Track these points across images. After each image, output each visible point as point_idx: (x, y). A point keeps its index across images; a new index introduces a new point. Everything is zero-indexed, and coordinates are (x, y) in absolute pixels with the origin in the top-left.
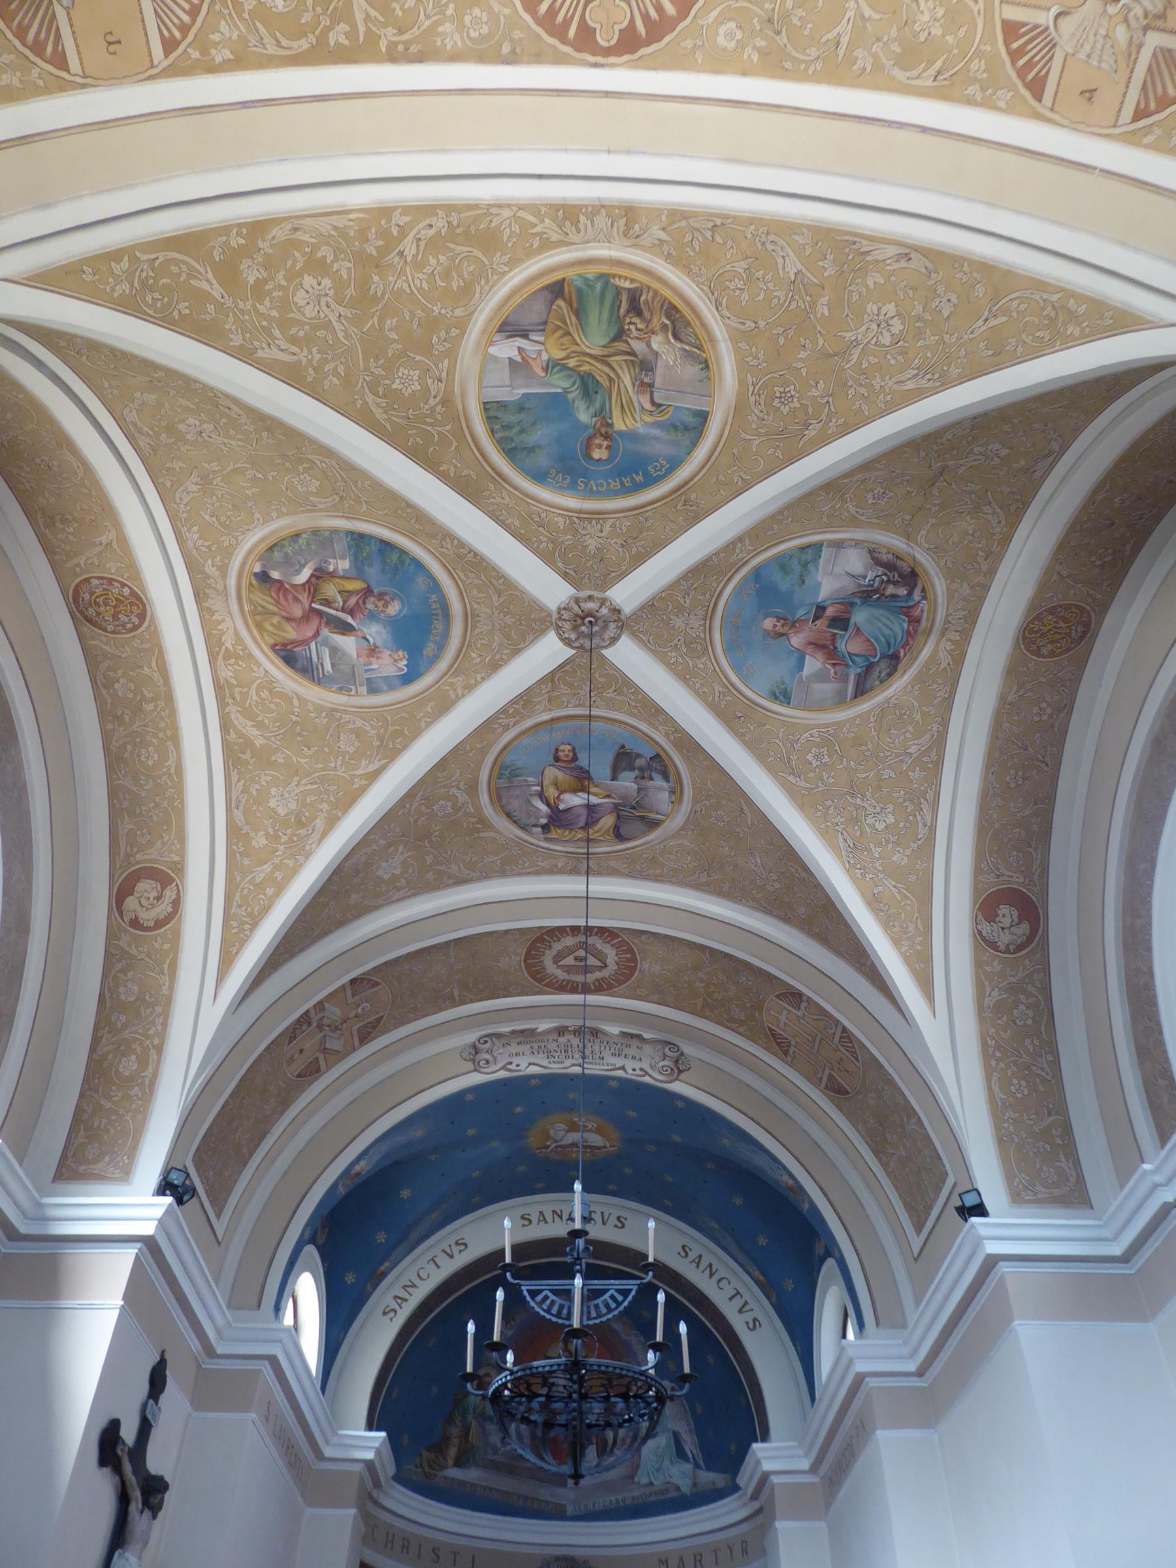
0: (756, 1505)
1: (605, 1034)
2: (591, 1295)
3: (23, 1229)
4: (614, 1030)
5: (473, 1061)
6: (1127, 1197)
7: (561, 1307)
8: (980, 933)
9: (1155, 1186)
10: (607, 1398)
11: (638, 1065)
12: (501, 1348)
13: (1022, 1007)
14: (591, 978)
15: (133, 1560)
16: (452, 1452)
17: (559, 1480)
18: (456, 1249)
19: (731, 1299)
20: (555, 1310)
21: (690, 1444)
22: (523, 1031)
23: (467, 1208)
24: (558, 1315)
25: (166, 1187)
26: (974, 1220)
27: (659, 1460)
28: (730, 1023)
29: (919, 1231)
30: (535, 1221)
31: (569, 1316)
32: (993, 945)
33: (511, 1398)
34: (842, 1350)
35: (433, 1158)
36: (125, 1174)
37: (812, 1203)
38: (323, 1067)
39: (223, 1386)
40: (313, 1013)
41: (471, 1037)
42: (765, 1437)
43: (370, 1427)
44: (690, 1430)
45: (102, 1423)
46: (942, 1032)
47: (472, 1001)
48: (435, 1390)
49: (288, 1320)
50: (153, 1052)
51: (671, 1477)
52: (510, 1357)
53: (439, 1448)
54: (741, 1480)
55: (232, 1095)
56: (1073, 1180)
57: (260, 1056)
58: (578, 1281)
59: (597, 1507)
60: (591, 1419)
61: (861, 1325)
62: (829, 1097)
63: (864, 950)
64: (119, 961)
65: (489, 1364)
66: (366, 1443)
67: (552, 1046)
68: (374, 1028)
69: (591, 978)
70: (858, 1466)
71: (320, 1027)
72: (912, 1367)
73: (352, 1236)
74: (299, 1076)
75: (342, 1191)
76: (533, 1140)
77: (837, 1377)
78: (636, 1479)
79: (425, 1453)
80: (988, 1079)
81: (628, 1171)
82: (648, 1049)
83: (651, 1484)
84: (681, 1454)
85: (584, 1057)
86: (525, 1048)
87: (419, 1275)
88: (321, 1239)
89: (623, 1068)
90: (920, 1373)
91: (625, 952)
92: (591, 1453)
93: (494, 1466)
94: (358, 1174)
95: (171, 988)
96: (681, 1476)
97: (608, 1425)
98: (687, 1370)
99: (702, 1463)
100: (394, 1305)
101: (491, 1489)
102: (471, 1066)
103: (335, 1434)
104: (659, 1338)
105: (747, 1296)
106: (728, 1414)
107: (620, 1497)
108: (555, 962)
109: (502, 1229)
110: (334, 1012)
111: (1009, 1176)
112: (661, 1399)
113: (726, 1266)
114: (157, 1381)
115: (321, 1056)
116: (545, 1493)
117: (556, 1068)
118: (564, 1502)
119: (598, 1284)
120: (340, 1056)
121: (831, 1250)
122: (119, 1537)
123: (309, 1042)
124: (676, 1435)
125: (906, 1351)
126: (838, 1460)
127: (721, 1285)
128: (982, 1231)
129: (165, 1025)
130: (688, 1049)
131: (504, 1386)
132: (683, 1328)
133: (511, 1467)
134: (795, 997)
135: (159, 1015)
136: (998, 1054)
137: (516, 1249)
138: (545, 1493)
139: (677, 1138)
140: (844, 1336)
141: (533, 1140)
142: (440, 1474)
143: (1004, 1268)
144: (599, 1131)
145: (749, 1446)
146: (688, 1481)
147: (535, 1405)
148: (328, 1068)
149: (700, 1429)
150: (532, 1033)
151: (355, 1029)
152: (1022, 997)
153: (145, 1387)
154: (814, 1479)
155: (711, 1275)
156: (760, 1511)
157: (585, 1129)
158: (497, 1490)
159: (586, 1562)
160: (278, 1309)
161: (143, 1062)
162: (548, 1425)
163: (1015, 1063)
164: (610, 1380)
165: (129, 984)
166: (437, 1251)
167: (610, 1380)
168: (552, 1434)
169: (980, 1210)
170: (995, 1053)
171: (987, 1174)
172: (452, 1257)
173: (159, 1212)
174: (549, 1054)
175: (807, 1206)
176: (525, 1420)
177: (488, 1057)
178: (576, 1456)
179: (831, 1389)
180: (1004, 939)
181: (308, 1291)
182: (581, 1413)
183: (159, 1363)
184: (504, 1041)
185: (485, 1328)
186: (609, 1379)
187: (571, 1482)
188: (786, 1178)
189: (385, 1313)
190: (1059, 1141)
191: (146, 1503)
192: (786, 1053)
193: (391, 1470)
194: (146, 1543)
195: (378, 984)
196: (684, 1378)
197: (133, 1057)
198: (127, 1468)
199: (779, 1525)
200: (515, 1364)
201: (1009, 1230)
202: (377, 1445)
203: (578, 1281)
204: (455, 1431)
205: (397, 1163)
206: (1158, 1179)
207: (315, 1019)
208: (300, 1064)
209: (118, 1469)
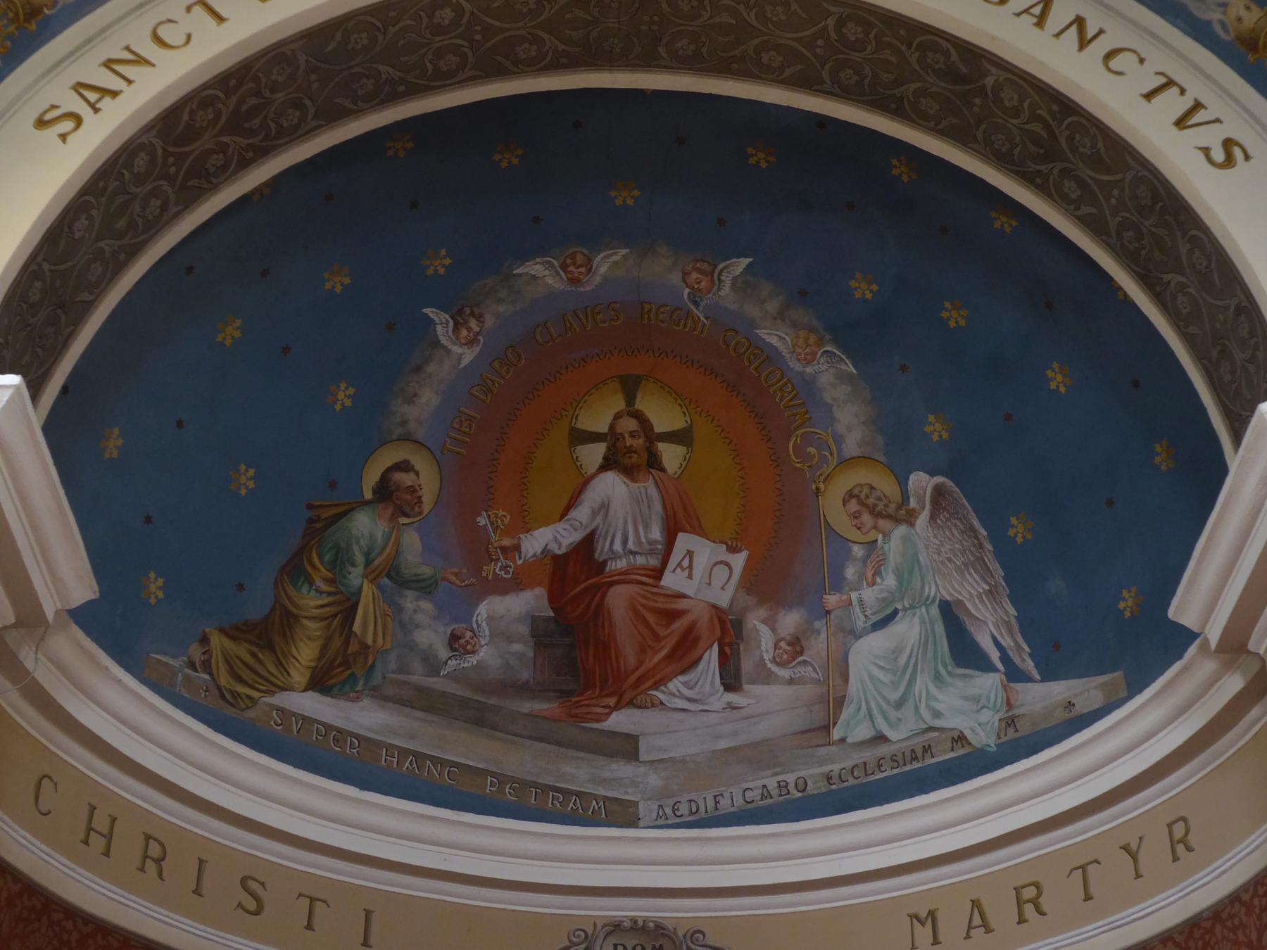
16: (305, 653)
19: (1149, 96)
21: (992, 625)
48: (246, 479)
51: (937, 714)
53: (268, 633)
54: (1185, 608)
59: (725, 803)
65: (407, 438)
78: (836, 734)
83: (881, 739)
84: (965, 652)
93: (428, 702)
99: (1029, 665)
105: (1197, 89)
107: (791, 778)
124: (951, 614)
127: (1115, 64)
146: (991, 718)
149: (1022, 585)
158: (436, 761)
159: (696, 934)
189: (41, 123)
204: (310, 601)
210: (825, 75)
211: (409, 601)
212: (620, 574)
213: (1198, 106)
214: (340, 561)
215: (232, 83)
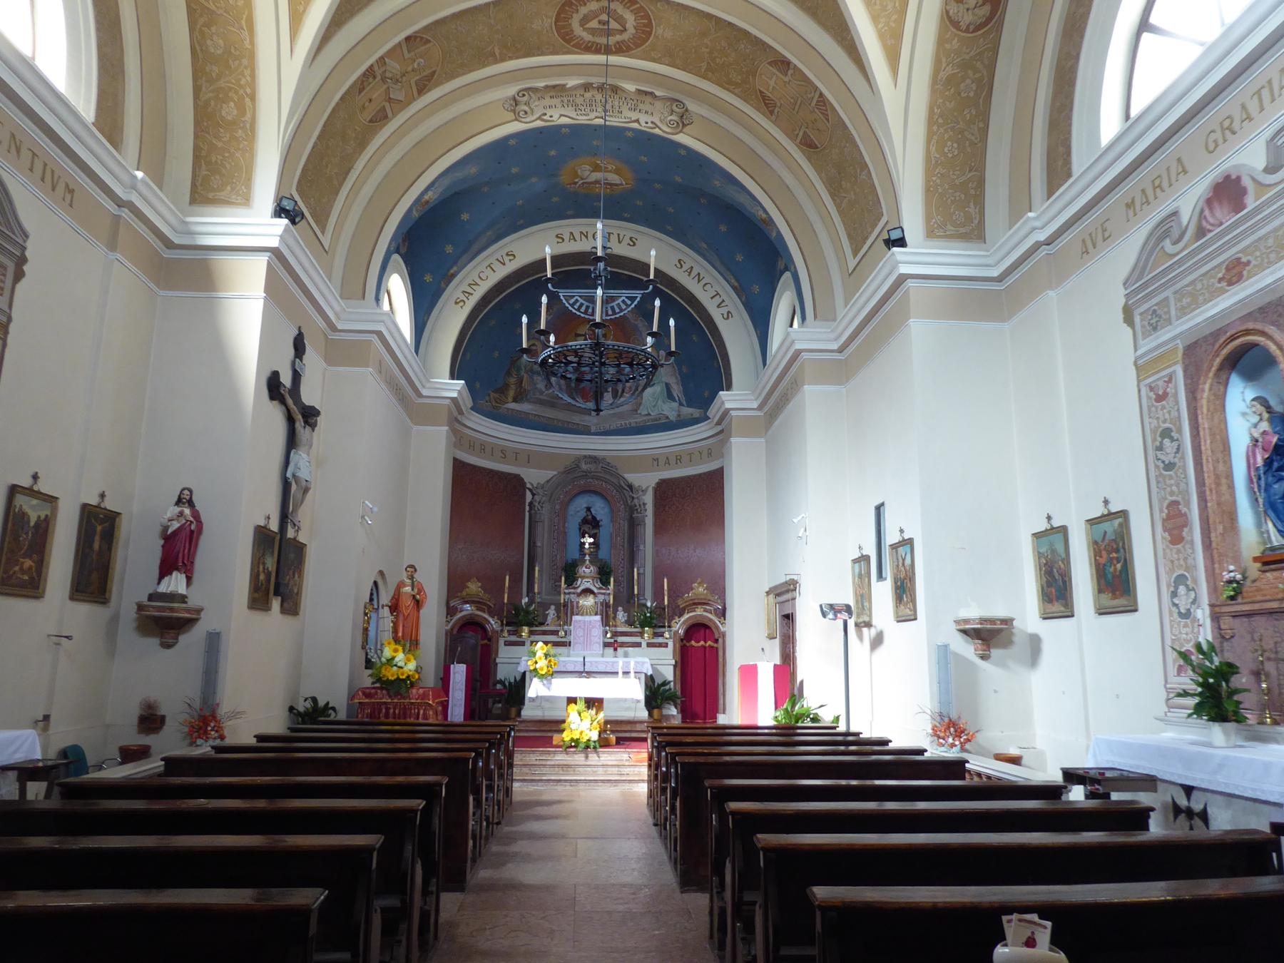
0: (719, 428)
1: (623, 90)
2: (606, 301)
3: (177, 241)
4: (631, 87)
5: (514, 111)
6: (1016, 232)
7: (588, 307)
8: (947, 12)
9: (1035, 229)
10: (618, 365)
11: (649, 119)
12: (545, 333)
13: (968, 81)
14: (612, 40)
15: (304, 455)
16: (511, 393)
17: (586, 412)
18: (507, 259)
20: (583, 309)
21: (677, 391)
22: (554, 87)
23: (515, 228)
24: (586, 313)
25: (280, 211)
26: (895, 249)
27: (654, 400)
28: (727, 84)
29: (855, 255)
30: (567, 239)
31: (593, 314)
32: (956, 24)
33: (554, 364)
34: (788, 334)
35: (486, 189)
36: (245, 200)
37: (779, 233)
38: (390, 115)
39: (346, 351)
40: (376, 68)
41: (511, 90)
42: (729, 387)
43: (452, 377)
45: (267, 374)
46: (899, 103)
47: (511, 58)
48: (496, 354)
49: (386, 307)
50: (247, 100)
52: (552, 338)
53: (503, 390)
55: (319, 138)
56: (976, 222)
57: (337, 104)
58: (599, 292)
60: (608, 377)
61: (803, 318)
62: (802, 151)
63: (847, 25)
64: (201, 15)
66: (454, 388)
67: (579, 100)
68: (429, 81)
69: (612, 40)
70: (790, 406)
71: (384, 79)
72: (835, 346)
73: (427, 246)
74: (371, 121)
75: (416, 214)
76: (564, 178)
77: (781, 353)
79: (493, 395)
80: (929, 141)
81: (639, 203)
82: (658, 104)
84: (670, 396)
85: (605, 111)
86: (556, 101)
87: (481, 275)
88: (403, 251)
89: (637, 121)
90: (841, 350)
91: (642, 17)
92: (608, 397)
94: (427, 202)
95: (252, 43)
96: (670, 410)
97: (619, 380)
98: (673, 349)
102: (512, 116)
104: (655, 329)
105: (724, 296)
106: (704, 370)
108: (582, 25)
109: (541, 245)
110: (394, 67)
111: (928, 218)
112: (654, 366)
113: (711, 275)
114: (299, 347)
115: (387, 105)
116: (577, 419)
117: (583, 120)
119: (612, 292)
120: (403, 104)
121: (789, 266)
122: (292, 441)
123: (376, 92)
124: (667, 385)
125: (833, 336)
126: (777, 403)
128: (899, 258)
129: (253, 76)
130: (692, 106)
131: (549, 356)
132: (672, 322)
133: (552, 403)
134: (784, 64)
135: (246, 67)
136: (940, 121)
137: (554, 258)
138: (577, 419)
139: (678, 179)
140: (791, 326)
141: (564, 178)
143: (910, 283)
144: (617, 172)
146: (675, 414)
147: (570, 368)
148: (394, 115)
149: (684, 382)
150: (562, 88)
151: (413, 82)
152: (970, 72)
153: (292, 351)
156: (722, 431)
157: (606, 170)
160: (377, 299)
161: (241, 108)
162: (579, 380)
163: (952, 129)
164: (621, 355)
165: (215, 38)
166: (492, 260)
167: (621, 355)
168: (582, 385)
169: (901, 242)
170: (937, 120)
171: (912, 218)
173: (280, 230)
174: (576, 107)
175: (774, 234)
176: (563, 377)
177: (526, 108)
178: (598, 398)
179: (779, 357)
180: (967, 18)
181: (397, 286)
182: (601, 373)
184: (539, 95)
185: (534, 320)
186: (620, 354)
187: (594, 413)
188: (761, 212)
190: (972, 192)
191: (306, 422)
192: (772, 113)
193: (469, 403)
194: (311, 446)
195: (428, 41)
196: (671, 354)
197: (232, 104)
198: (290, 401)
199: (732, 440)
200: (556, 343)
201: (923, 256)
203: (599, 292)
204: (512, 380)
205: (456, 193)
206: (1037, 224)
207: (378, 72)
208: (371, 110)
209: (283, 401)
211: (535, 377)
212: (425, 915)
214: (519, 369)
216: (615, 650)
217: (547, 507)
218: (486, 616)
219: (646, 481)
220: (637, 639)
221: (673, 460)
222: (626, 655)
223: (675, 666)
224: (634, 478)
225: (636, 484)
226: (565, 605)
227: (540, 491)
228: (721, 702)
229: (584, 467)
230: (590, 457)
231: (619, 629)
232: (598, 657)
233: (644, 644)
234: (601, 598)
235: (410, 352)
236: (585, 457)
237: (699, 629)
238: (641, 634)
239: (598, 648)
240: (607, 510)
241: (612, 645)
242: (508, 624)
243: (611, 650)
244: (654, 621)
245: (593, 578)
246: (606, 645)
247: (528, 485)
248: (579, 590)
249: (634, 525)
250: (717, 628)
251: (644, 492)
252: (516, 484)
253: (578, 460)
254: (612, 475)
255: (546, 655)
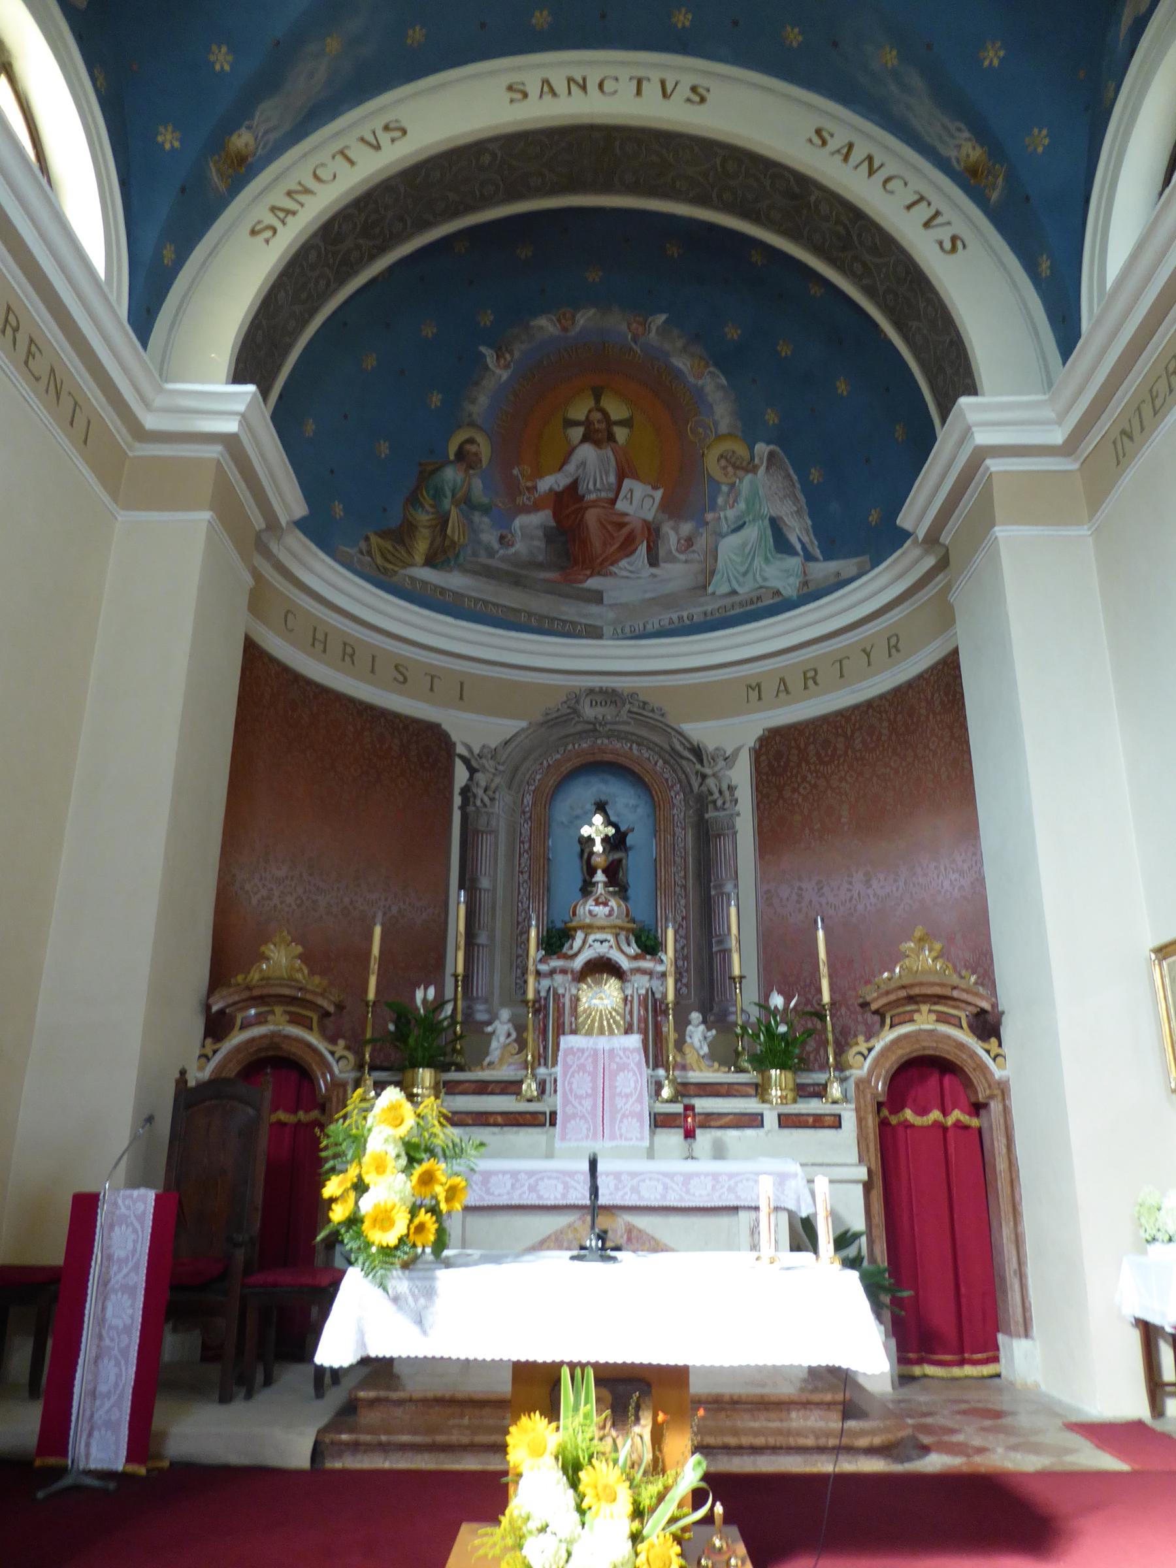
16: (421, 547)
21: (798, 530)
42: (972, 390)
44: (799, 512)
48: (384, 448)
51: (765, 579)
53: (402, 535)
65: (472, 424)
78: (710, 590)
79: (374, 539)
83: (734, 592)
84: (782, 545)
93: (488, 573)
99: (817, 553)
100: (270, 219)
101: (486, 603)
103: (160, 390)
105: (938, 203)
118: (598, 623)
127: (890, 186)
142: (403, 571)
145: (954, 402)
146: (794, 581)
154: (1068, 465)
155: (871, 172)
158: (494, 604)
166: (350, 140)
172: (378, 147)
183: (657, 1242)
189: (253, 232)
199: (1000, 531)
202: (241, 408)
204: (423, 518)
210: (714, 195)
211: (477, 517)
213: (937, 214)
214: (438, 494)
215: (362, 204)
216: (689, 1134)
217: (505, 799)
218: (313, 1039)
219: (731, 738)
220: (750, 1105)
221: (795, 683)
222: (719, 1152)
223: (868, 1187)
224: (704, 732)
225: (710, 745)
226: (540, 1008)
227: (489, 764)
228: (1014, 1296)
229: (589, 712)
230: (603, 691)
231: (695, 1076)
232: (645, 1166)
233: (771, 1119)
234: (640, 984)
235: (105, 318)
236: (591, 691)
237: (924, 1074)
238: (760, 1090)
239: (637, 1130)
240: (643, 810)
241: (680, 1120)
242: (373, 1068)
243: (673, 1138)
244: (792, 1050)
245: (617, 930)
246: (660, 1122)
247: (460, 750)
248: (578, 963)
249: (708, 837)
250: (983, 1068)
251: (730, 760)
252: (429, 747)
253: (574, 699)
254: (653, 728)
255: (414, 1153)
